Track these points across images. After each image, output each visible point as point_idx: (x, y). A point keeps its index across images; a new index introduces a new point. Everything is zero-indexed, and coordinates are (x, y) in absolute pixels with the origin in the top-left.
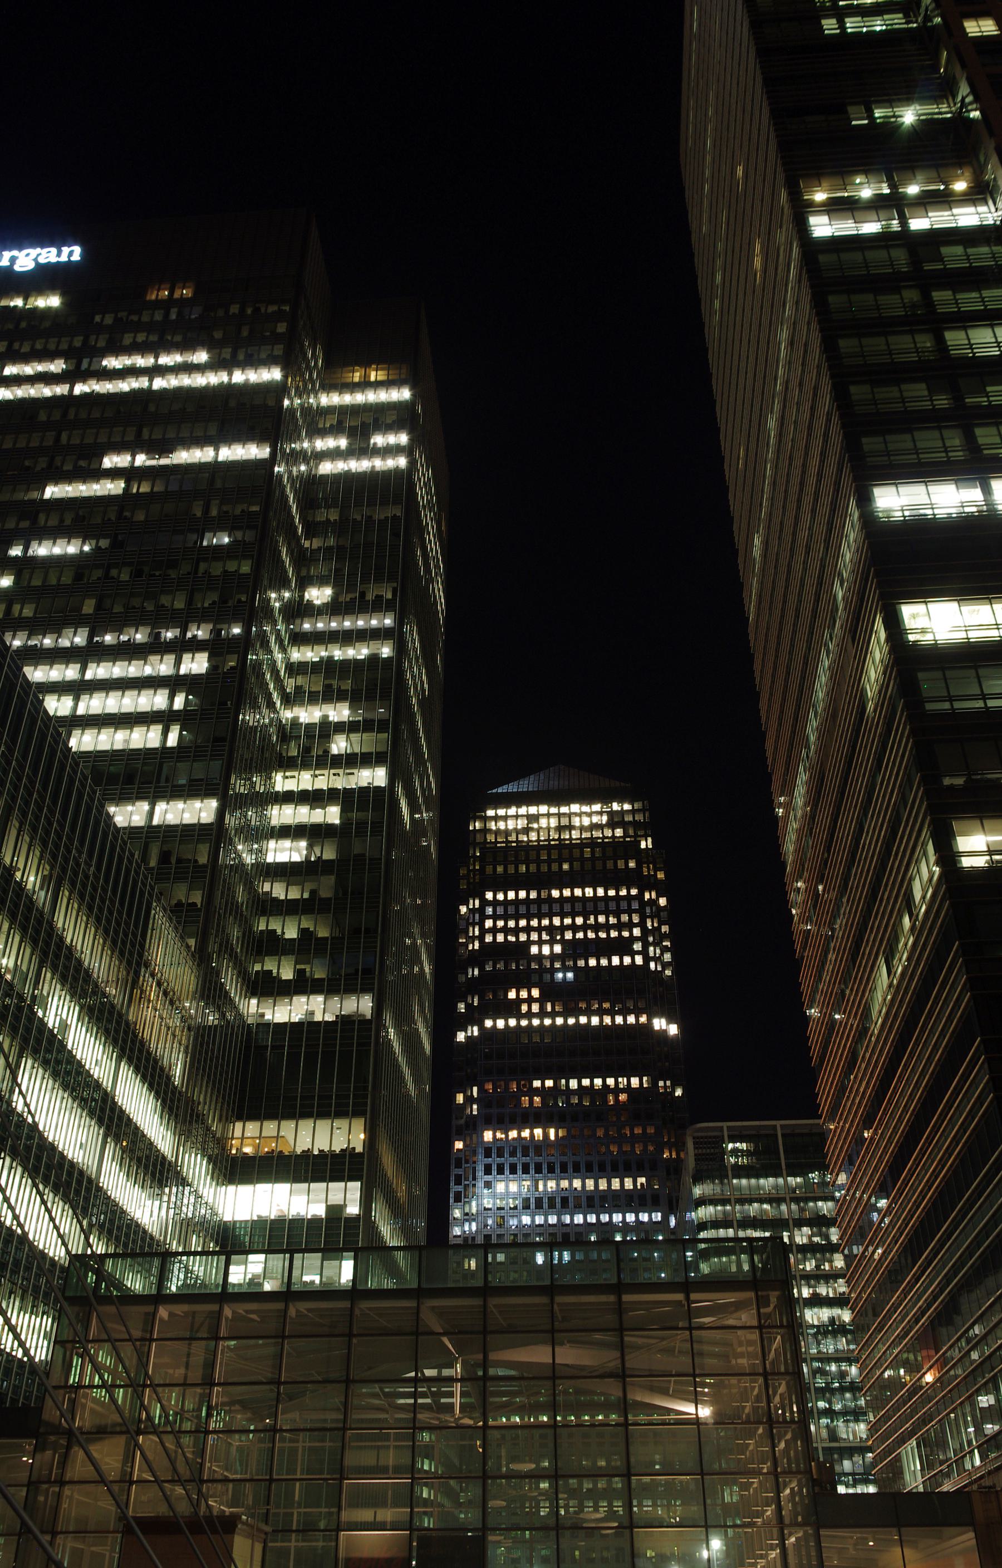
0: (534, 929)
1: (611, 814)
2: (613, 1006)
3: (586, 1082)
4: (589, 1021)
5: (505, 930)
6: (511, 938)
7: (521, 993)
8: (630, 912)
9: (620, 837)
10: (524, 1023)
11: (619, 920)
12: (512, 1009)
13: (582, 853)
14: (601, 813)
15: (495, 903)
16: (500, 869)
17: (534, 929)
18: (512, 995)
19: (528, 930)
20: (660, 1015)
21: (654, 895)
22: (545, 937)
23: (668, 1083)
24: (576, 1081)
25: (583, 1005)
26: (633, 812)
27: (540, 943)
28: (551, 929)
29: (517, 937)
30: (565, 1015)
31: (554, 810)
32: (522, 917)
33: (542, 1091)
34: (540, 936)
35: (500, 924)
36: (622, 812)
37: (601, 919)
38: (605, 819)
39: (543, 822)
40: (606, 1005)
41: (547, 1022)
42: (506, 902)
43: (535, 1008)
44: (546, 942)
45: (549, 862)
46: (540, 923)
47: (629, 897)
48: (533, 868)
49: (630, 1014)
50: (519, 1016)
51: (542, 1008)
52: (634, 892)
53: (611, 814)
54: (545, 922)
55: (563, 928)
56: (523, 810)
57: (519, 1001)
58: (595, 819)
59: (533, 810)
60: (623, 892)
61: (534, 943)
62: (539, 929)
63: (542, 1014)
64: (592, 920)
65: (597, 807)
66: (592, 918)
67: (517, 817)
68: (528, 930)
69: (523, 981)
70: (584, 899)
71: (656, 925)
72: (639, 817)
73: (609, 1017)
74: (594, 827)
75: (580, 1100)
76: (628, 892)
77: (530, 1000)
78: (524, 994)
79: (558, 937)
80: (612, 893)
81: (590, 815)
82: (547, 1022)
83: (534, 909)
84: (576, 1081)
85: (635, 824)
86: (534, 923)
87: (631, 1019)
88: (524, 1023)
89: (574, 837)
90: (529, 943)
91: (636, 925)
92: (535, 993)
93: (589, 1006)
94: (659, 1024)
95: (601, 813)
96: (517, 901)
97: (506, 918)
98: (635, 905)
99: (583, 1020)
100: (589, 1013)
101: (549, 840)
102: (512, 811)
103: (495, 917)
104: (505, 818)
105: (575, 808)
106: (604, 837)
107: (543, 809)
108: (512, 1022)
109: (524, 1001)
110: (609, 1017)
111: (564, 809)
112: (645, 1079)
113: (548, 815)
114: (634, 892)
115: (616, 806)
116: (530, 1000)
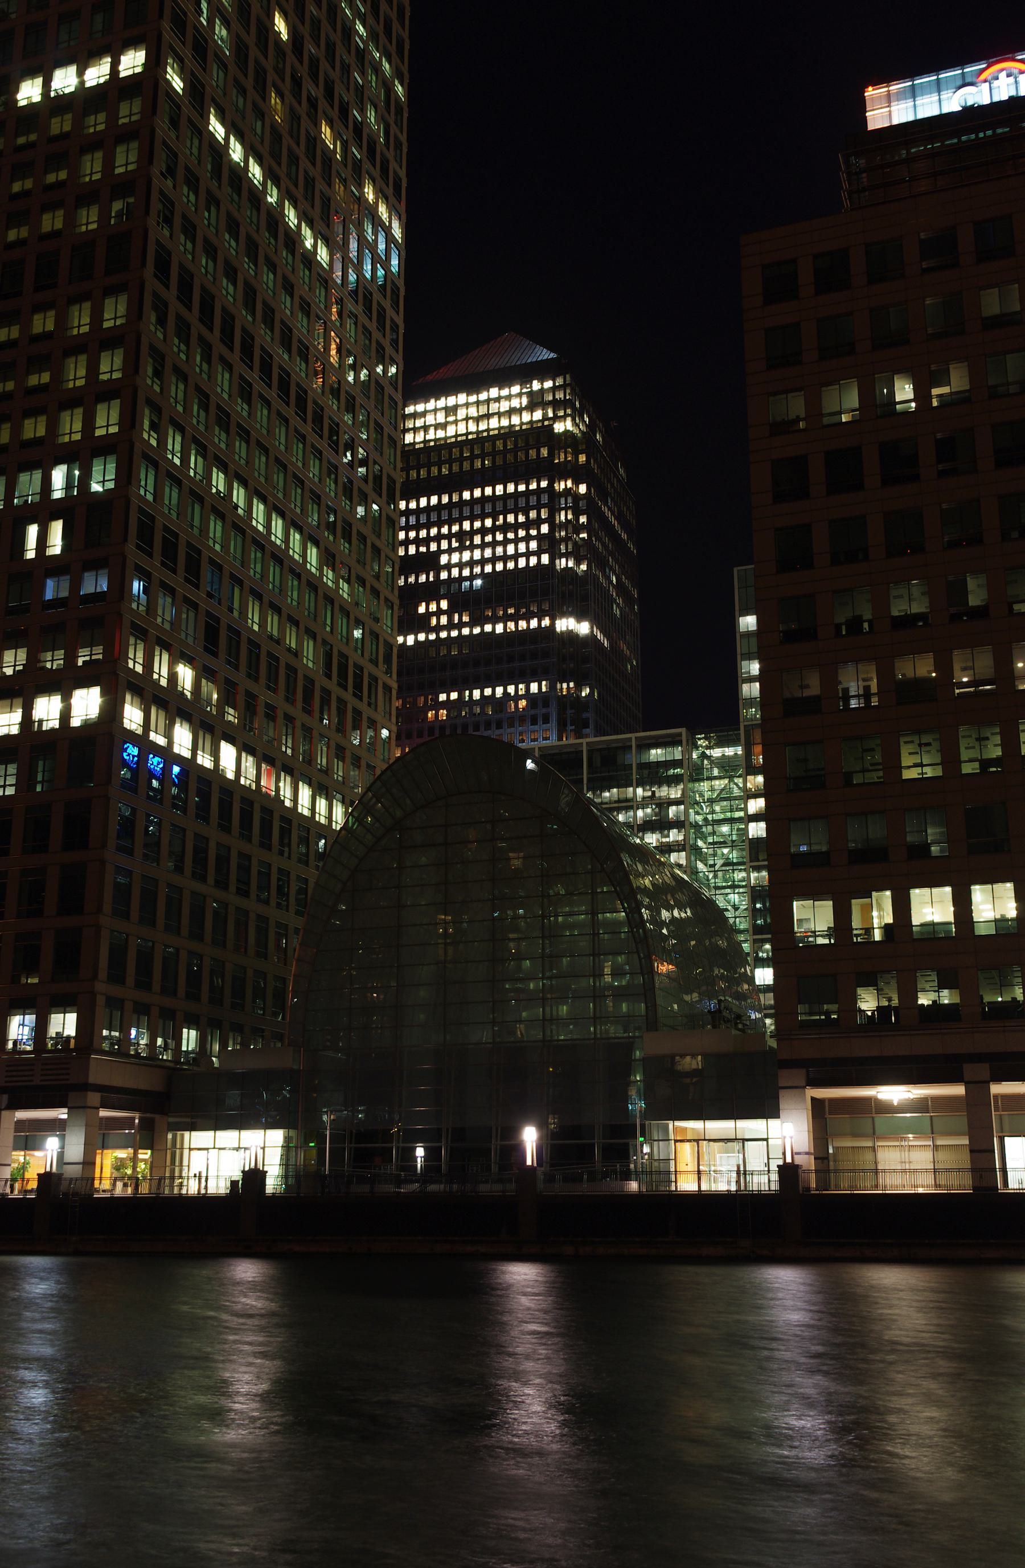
0: (444, 537)
1: (531, 394)
2: (517, 611)
3: (488, 692)
4: (494, 629)
5: (417, 542)
6: (423, 549)
7: (431, 607)
8: (538, 508)
9: (539, 421)
10: (432, 637)
11: (527, 517)
12: (422, 623)
13: (494, 445)
14: (520, 395)
15: (408, 512)
16: (423, 473)
17: (444, 537)
18: (422, 609)
19: (439, 538)
20: (564, 614)
21: (569, 484)
22: (455, 544)
23: (572, 685)
24: (479, 691)
25: (534, 608)
26: (554, 389)
27: (450, 551)
28: (461, 535)
29: (428, 548)
30: (471, 625)
31: (473, 398)
32: (488, 516)
33: (448, 703)
34: (450, 544)
35: (412, 534)
36: (542, 391)
37: (511, 518)
38: (525, 401)
39: (462, 413)
40: (511, 611)
41: (454, 633)
42: (418, 511)
43: (444, 620)
44: (455, 550)
45: (515, 450)
46: (450, 529)
47: (539, 490)
48: (455, 468)
49: (533, 618)
50: (429, 630)
51: (450, 619)
52: (544, 484)
53: (531, 394)
54: (455, 528)
55: (473, 532)
56: (441, 403)
57: (428, 614)
58: (515, 403)
59: (451, 401)
60: (533, 486)
61: (444, 552)
62: (449, 537)
63: (450, 626)
64: (501, 521)
65: (516, 389)
66: (501, 517)
67: (435, 411)
68: (439, 538)
69: (431, 592)
70: (494, 497)
71: (570, 517)
72: (560, 395)
73: (513, 623)
74: (511, 412)
75: (482, 709)
76: (538, 485)
77: (439, 612)
78: (433, 607)
79: (468, 543)
80: (522, 488)
81: (509, 398)
82: (454, 633)
83: (477, 510)
84: (479, 691)
85: (555, 404)
86: (445, 530)
87: (534, 623)
88: (432, 637)
89: (491, 427)
90: (440, 552)
91: (544, 521)
92: (444, 605)
93: (494, 613)
94: (565, 624)
95: (520, 395)
96: (429, 508)
97: (417, 528)
98: (545, 499)
99: (488, 628)
100: (494, 621)
101: (467, 434)
102: (431, 405)
103: (407, 529)
104: (424, 414)
105: (494, 392)
106: (522, 424)
107: (462, 398)
108: (422, 637)
109: (433, 614)
110: (513, 623)
111: (483, 396)
112: (544, 683)
113: (467, 405)
114: (544, 484)
115: (536, 385)
116: (439, 612)
